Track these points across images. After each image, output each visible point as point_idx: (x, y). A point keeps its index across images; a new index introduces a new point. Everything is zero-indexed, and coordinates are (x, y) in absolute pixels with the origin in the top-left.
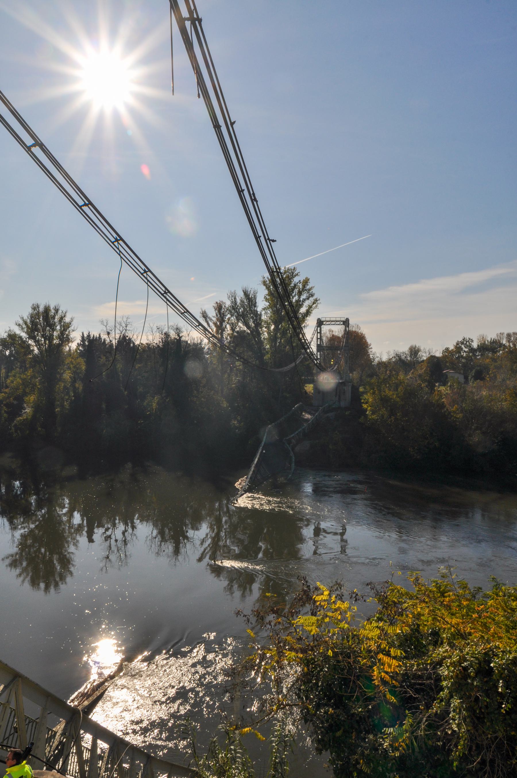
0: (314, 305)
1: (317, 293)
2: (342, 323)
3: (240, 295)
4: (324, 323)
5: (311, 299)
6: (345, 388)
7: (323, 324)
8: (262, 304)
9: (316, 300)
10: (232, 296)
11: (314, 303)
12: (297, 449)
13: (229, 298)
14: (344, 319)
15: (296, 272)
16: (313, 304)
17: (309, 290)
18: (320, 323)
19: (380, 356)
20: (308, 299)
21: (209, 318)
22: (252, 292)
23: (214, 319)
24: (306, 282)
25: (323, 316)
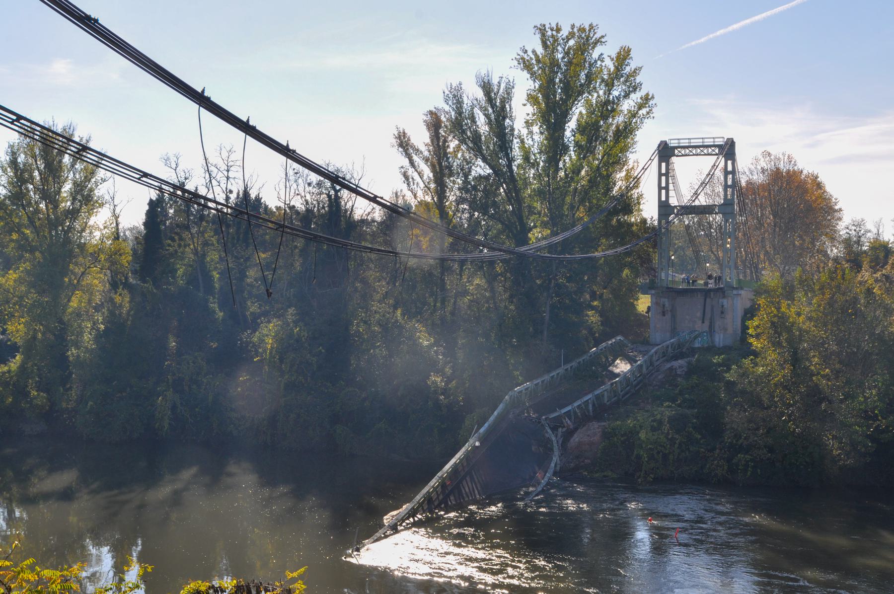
0: (643, 111)
1: (647, 82)
2: (717, 151)
3: (473, 93)
4: (676, 151)
5: (632, 96)
6: (725, 301)
7: (674, 155)
8: (521, 112)
9: (647, 99)
10: (455, 96)
11: (640, 107)
12: (576, 439)
13: (446, 101)
14: (720, 142)
15: (597, 36)
16: (640, 108)
17: (629, 76)
18: (665, 152)
19: (875, 231)
20: (627, 96)
21: (413, 147)
22: (503, 86)
23: (426, 154)
24: (623, 57)
25: (672, 136)
